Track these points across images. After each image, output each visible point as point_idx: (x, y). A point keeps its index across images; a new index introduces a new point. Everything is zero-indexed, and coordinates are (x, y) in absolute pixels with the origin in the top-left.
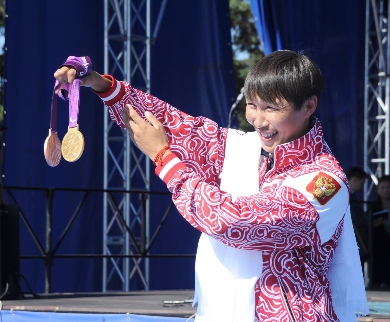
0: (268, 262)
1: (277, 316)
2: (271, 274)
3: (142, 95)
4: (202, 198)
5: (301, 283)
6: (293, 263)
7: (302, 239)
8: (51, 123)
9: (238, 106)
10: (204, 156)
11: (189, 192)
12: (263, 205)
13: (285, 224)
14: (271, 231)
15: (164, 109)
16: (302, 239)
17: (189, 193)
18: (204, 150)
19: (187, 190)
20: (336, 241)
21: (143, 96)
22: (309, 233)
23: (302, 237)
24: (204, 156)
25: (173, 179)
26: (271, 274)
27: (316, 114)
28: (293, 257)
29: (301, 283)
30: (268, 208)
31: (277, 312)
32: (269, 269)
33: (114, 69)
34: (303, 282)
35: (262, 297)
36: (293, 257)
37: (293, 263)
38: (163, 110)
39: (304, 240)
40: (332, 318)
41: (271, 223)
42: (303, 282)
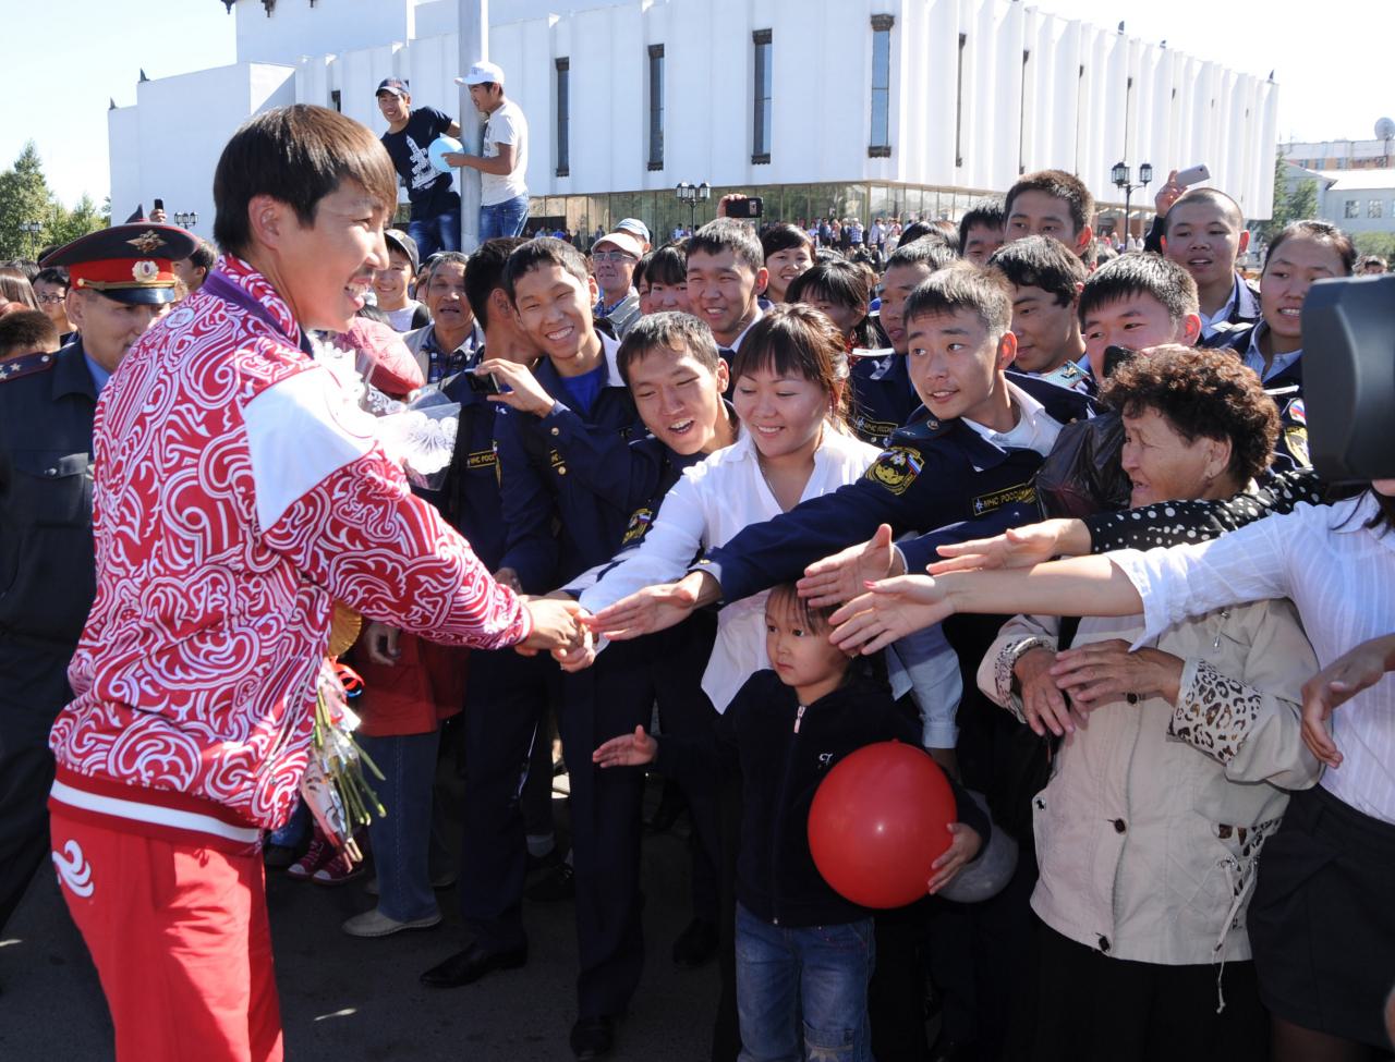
0: (197, 451)
1: (182, 577)
2: (194, 483)
3: (296, 532)
6: (174, 707)
9: (282, 132)
10: (204, 413)
12: (198, 656)
13: (205, 690)
18: (189, 411)
21: (294, 527)
22: (153, 574)
24: (204, 413)
26: (194, 483)
27: (283, 145)
28: (174, 755)
30: (209, 673)
31: (184, 567)
32: (194, 469)
35: (202, 437)
36: (174, 755)
37: (174, 707)
40: (197, 383)
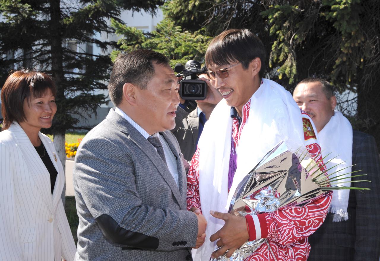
1: (260, 250)
4: (294, 221)
5: (284, 227)
7: (295, 214)
8: (358, 176)
11: (287, 224)
14: (279, 213)
15: (292, 236)
16: (295, 214)
17: (289, 225)
19: (285, 224)
20: (304, 124)
23: (295, 216)
25: (270, 226)
29: (284, 227)
33: (377, 49)
34: (283, 225)
38: (291, 237)
39: (293, 214)
41: (133, 46)
42: (283, 225)
